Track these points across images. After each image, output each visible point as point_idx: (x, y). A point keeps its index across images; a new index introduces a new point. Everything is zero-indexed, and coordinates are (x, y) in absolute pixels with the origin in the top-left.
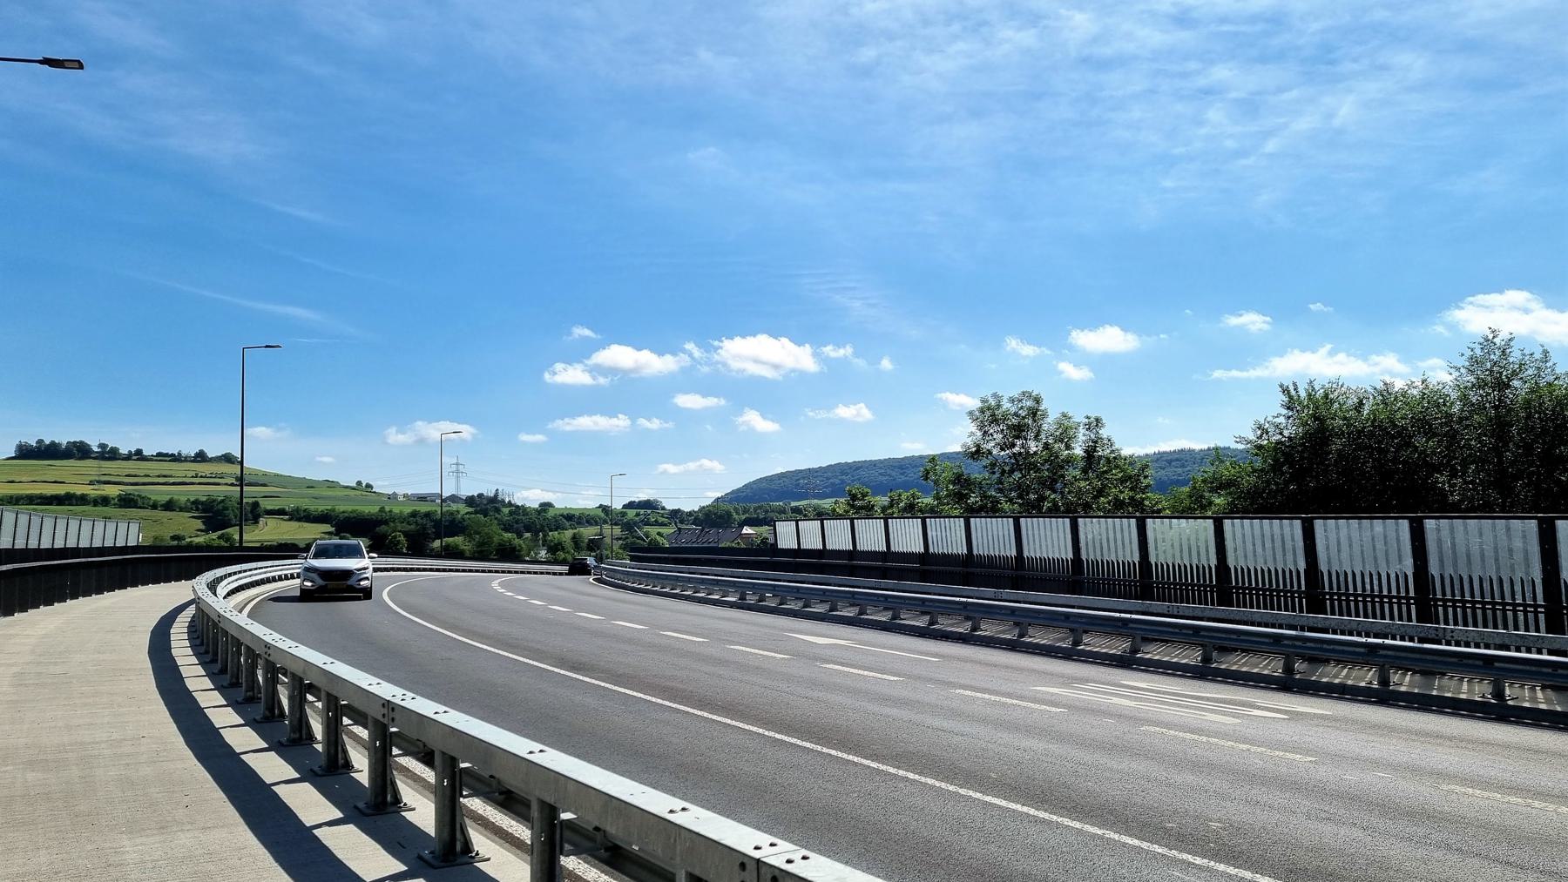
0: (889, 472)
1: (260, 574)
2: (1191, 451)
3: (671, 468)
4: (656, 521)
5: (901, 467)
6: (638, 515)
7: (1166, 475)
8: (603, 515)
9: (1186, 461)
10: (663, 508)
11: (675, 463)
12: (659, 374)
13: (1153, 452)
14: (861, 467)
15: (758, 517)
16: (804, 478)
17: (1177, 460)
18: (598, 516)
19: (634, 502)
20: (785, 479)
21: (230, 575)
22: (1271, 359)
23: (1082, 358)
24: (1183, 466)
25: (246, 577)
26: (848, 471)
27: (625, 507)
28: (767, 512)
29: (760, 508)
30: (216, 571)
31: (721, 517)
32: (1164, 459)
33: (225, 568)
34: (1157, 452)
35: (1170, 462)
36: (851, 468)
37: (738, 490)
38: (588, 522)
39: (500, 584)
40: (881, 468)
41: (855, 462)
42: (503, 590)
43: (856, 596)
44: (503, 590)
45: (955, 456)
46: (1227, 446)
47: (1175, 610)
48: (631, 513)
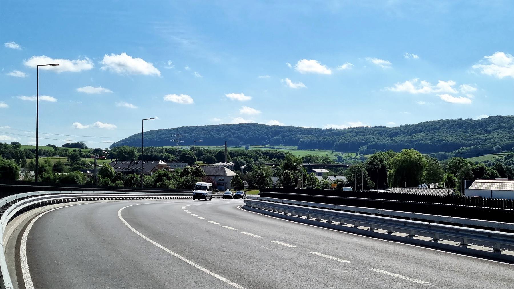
0: (211, 132)
1: (41, 199)
2: (367, 128)
3: (80, 126)
4: (86, 155)
5: (217, 130)
6: (74, 151)
7: (356, 140)
8: (53, 151)
9: (366, 133)
10: (86, 148)
11: (83, 123)
12: (118, 70)
13: (348, 128)
14: (195, 129)
15: (147, 155)
16: (163, 134)
17: (361, 132)
18: (51, 151)
19: (69, 144)
20: (152, 134)
21: (19, 200)
22: (112, 54)
23: (297, 77)
24: (364, 135)
25: (20, 205)
26: (188, 131)
27: (63, 146)
28: (152, 152)
29: (148, 149)
30: (8, 198)
31: (128, 154)
32: (355, 131)
33: (16, 195)
34: (350, 127)
35: (357, 133)
36: (190, 130)
37: (126, 139)
38: (44, 154)
39: (186, 208)
40: (206, 130)
41: (192, 126)
42: (189, 212)
43: (326, 213)
44: (189, 212)
45: (247, 126)
46: (384, 126)
47: (450, 219)
48: (71, 150)
